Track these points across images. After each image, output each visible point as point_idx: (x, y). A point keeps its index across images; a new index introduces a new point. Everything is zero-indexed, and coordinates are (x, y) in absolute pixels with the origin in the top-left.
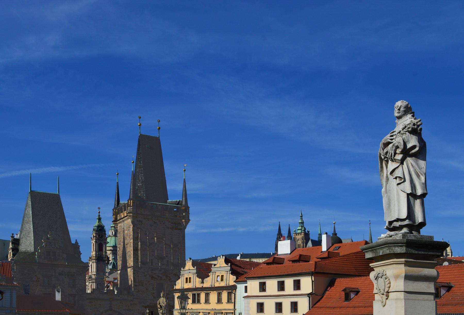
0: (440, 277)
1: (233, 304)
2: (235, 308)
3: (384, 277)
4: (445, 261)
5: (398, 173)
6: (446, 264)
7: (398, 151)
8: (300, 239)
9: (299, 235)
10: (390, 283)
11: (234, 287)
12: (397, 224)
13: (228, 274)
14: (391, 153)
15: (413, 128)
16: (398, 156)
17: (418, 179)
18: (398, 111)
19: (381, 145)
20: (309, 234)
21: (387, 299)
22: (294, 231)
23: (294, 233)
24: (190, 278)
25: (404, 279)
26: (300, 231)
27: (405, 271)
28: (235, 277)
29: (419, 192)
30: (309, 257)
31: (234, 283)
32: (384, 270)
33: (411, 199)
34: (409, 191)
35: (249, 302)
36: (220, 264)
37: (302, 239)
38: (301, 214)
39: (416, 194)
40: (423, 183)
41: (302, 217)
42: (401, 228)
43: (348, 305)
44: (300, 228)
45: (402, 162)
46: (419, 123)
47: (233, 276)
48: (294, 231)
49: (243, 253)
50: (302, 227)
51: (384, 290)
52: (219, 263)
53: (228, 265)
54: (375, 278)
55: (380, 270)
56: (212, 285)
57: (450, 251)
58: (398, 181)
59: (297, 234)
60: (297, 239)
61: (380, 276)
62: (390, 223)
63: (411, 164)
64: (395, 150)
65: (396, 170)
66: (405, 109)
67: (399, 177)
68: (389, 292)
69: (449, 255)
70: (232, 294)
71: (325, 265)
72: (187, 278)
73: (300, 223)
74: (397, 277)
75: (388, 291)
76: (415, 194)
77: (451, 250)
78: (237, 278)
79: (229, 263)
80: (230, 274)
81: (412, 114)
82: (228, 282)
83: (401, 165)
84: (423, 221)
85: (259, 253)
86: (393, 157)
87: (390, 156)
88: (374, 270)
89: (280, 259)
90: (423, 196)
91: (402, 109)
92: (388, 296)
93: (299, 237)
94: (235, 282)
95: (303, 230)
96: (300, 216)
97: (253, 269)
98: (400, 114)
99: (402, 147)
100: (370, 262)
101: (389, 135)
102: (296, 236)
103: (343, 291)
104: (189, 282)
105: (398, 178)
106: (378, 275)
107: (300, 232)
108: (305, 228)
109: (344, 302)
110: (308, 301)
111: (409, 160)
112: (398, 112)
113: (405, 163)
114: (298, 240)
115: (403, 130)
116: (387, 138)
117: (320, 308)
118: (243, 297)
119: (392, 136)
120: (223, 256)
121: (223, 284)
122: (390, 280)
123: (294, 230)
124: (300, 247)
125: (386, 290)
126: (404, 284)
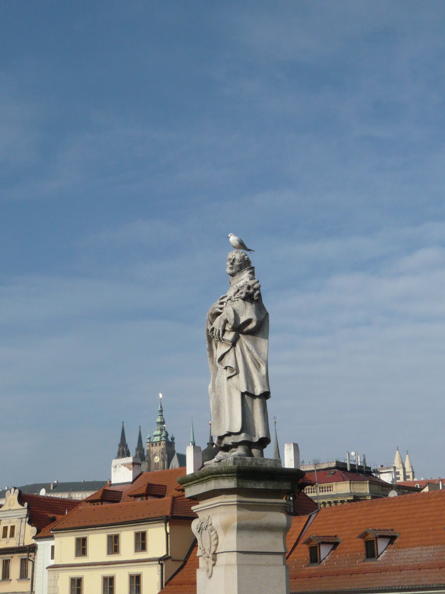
0: (293, 525)
1: (30, 582)
2: (33, 591)
3: (209, 528)
4: (392, 489)
5: (229, 361)
6: (393, 494)
7: (228, 327)
8: (159, 453)
9: (156, 446)
10: (217, 538)
11: (33, 549)
12: (228, 441)
13: (23, 524)
14: (218, 329)
15: (247, 293)
16: (228, 336)
17: (256, 371)
18: (231, 266)
19: (207, 316)
21: (214, 565)
22: (148, 439)
23: (147, 443)
24: (13, 528)
25: (237, 530)
26: (157, 439)
27: (238, 519)
28: (35, 529)
29: (259, 390)
30: (165, 487)
31: (33, 541)
32: (209, 517)
34: (244, 390)
35: (56, 578)
36: (9, 504)
37: (162, 453)
38: (160, 407)
39: (254, 393)
40: (263, 376)
41: (161, 411)
42: (235, 445)
44: (158, 432)
45: (234, 345)
46: (255, 286)
47: (32, 526)
48: (148, 439)
49: (57, 482)
50: (161, 430)
51: (209, 550)
52: (8, 503)
53: (23, 505)
54: (198, 530)
55: (203, 517)
56: (19, 543)
57: (411, 470)
58: (228, 373)
59: (152, 444)
60: (153, 454)
61: (204, 527)
62: (221, 438)
63: (247, 347)
64: (224, 326)
65: (226, 356)
66: (240, 263)
67: (230, 367)
68: (216, 554)
69: (409, 477)
70: (28, 561)
71: (189, 503)
72: (5, 528)
73: (158, 423)
74: (226, 528)
75: (215, 551)
76: (252, 393)
77: (412, 467)
78: (38, 531)
79: (25, 502)
80: (26, 522)
81: (251, 271)
82: (22, 539)
83: (233, 347)
84: (265, 436)
85: (85, 481)
86: (221, 336)
87: (217, 334)
88: (198, 517)
89: (114, 493)
90: (265, 395)
91: (236, 263)
92: (215, 560)
93: (156, 449)
94: (35, 538)
95: (164, 437)
96: (159, 409)
97: (68, 512)
98: (234, 270)
99: (232, 322)
100: (191, 504)
101: (218, 302)
102: (152, 448)
104: (10, 537)
105: (228, 368)
106: (201, 526)
107: (158, 440)
108: (166, 432)
110: (160, 573)
111: (245, 341)
112: (230, 268)
113: (238, 346)
114: (155, 455)
115: (235, 295)
116: (216, 306)
117: (181, 585)
118: (47, 568)
119: (222, 303)
120: (15, 488)
121: (12, 543)
122: (218, 533)
123: (148, 437)
125: (212, 551)
126: (237, 540)
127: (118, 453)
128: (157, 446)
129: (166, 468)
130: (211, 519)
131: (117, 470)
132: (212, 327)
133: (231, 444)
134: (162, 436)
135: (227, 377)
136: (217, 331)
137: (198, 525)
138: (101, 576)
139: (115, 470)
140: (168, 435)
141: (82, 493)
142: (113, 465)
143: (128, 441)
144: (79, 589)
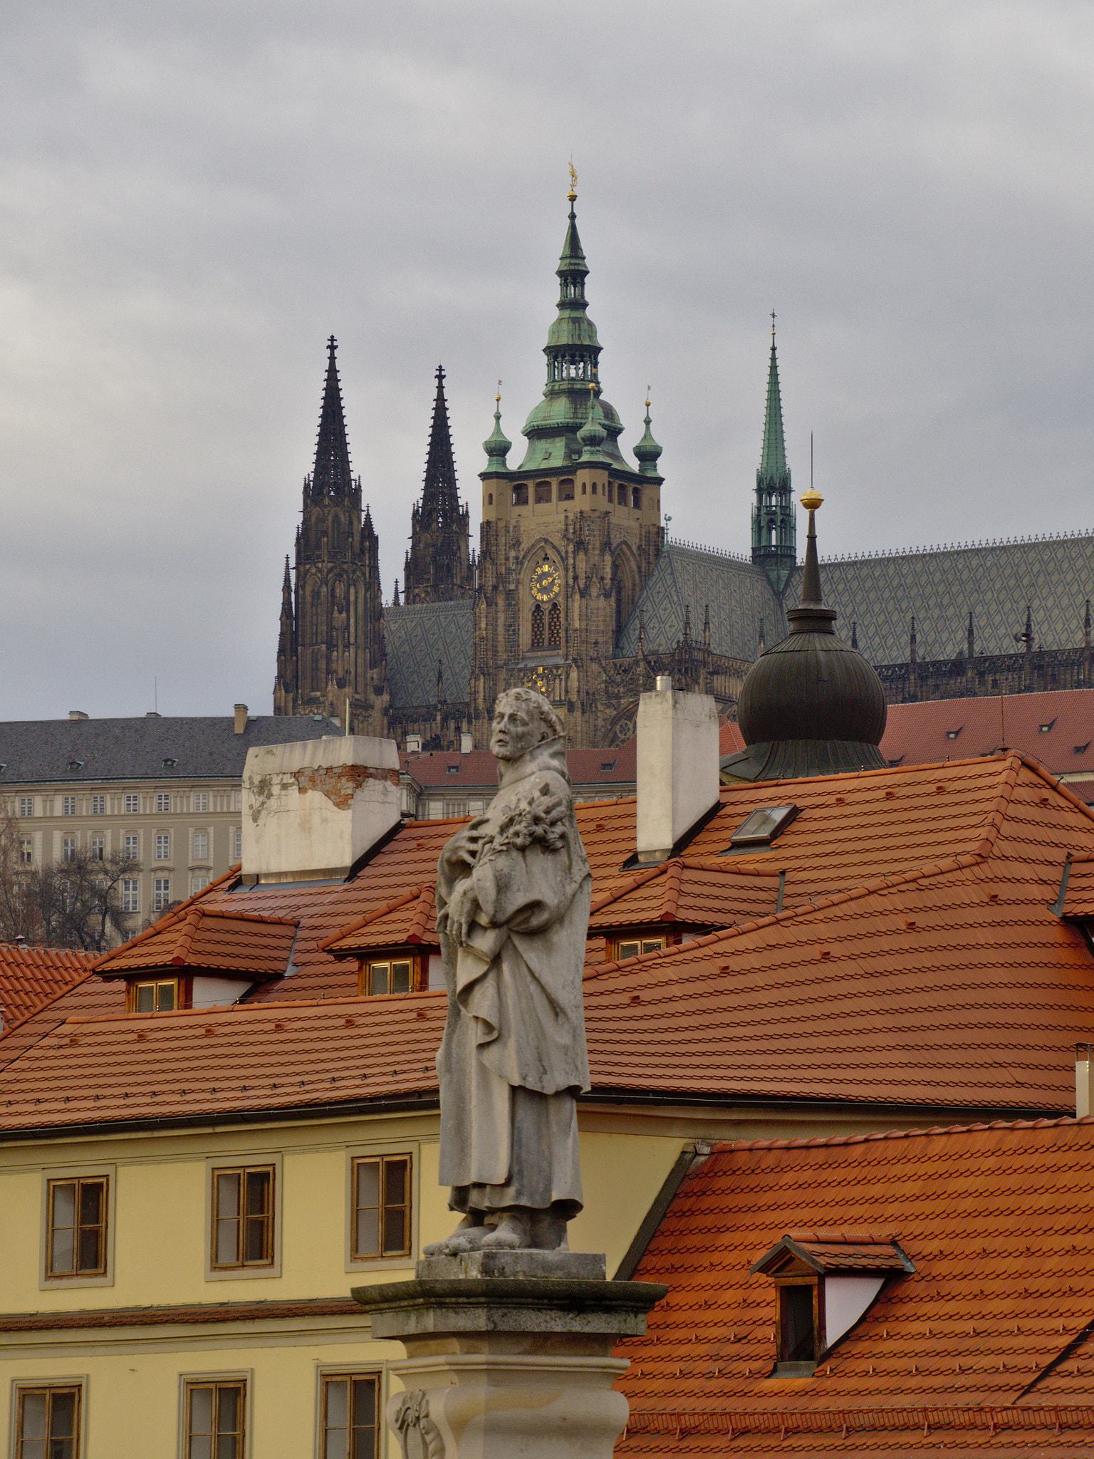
5: (483, 1003)
8: (556, 539)
20: (659, 481)
33: (527, 1115)
43: (801, 1403)
45: (496, 961)
61: (410, 1420)
98: (509, 748)
103: (764, 1268)
107: (557, 461)
109: (770, 1375)
112: (500, 741)
119: (474, 840)
124: (553, 645)
127: (298, 539)
128: (549, 500)
129: (463, 935)
130: (427, 1401)
131: (273, 803)
132: (443, 911)
133: (485, 1209)
134: (580, 434)
135: (478, 1043)
136: (456, 926)
137: (399, 1412)
138: (176, 1378)
139: (263, 803)
140: (620, 431)
141: (70, 795)
142: (250, 778)
143: (360, 465)
144: (61, 1442)
